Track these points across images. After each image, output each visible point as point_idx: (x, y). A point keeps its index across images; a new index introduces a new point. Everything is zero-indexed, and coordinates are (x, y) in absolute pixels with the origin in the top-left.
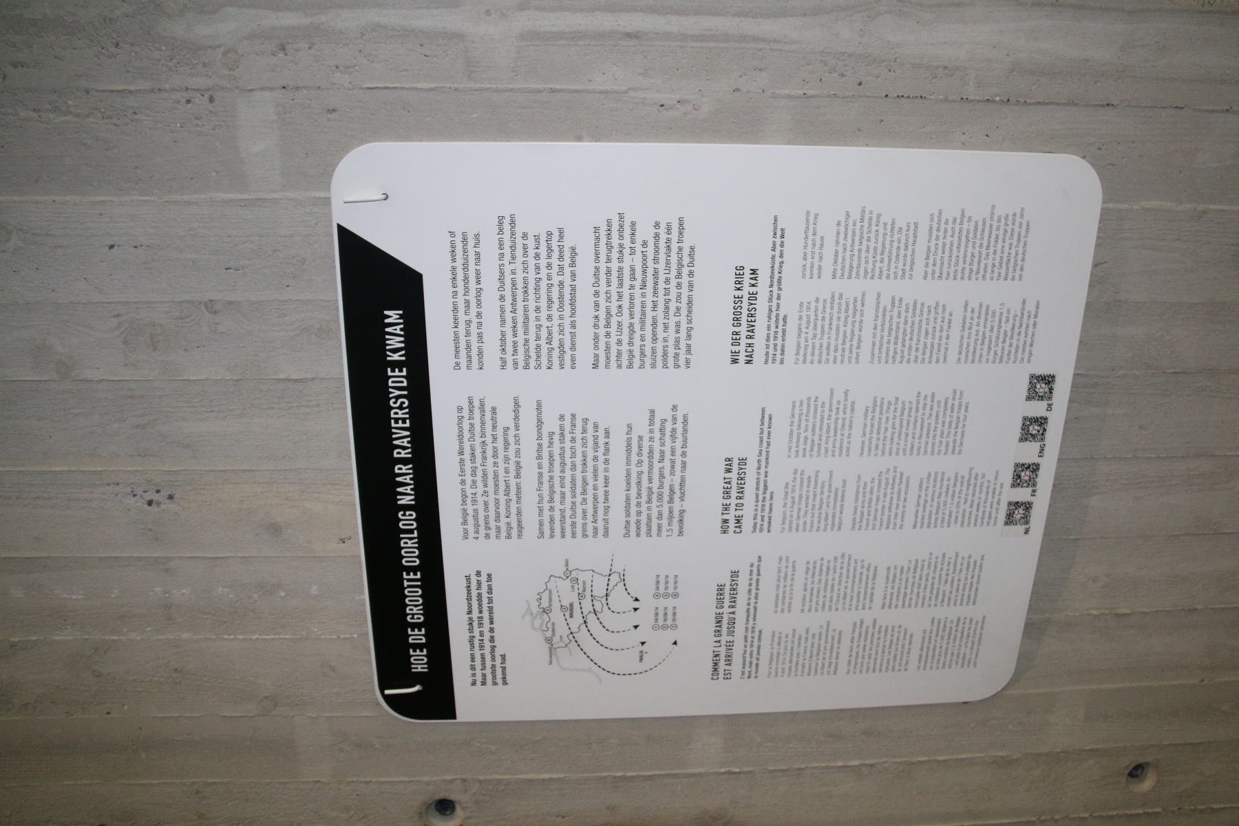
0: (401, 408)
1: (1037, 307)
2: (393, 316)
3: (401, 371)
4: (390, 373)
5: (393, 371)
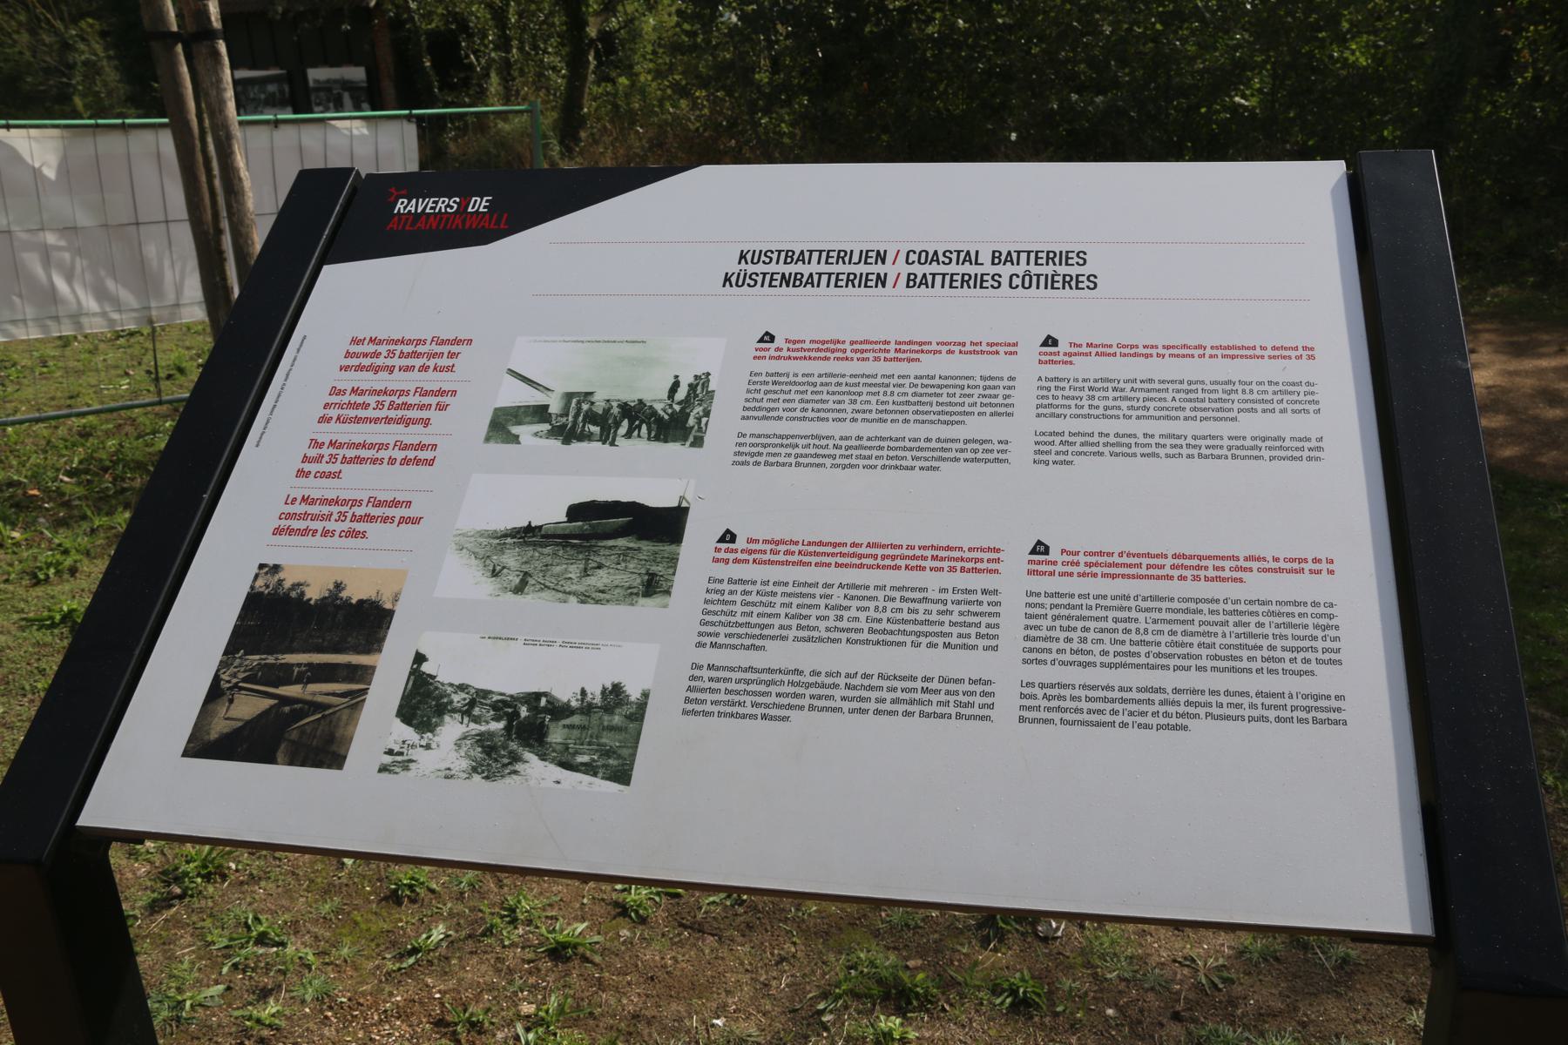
0: (448, 206)
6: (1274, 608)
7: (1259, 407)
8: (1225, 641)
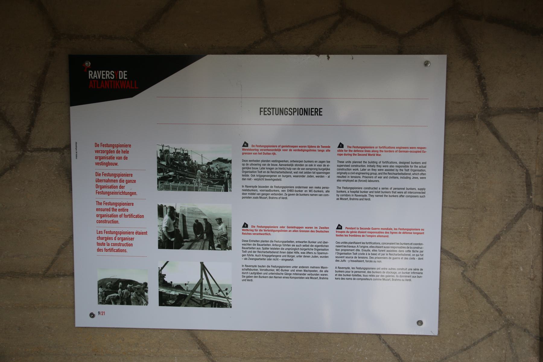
0: (110, 75)
1: (138, 216)
2: (123, 75)
3: (126, 77)
4: (124, 72)
5: (126, 73)
6: (252, 196)
7: (399, 176)
8: (369, 252)
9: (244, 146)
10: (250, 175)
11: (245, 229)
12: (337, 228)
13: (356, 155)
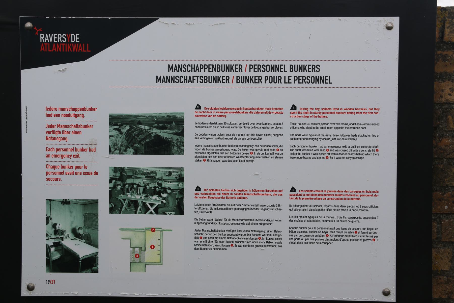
0: (62, 39)
2: (75, 38)
3: (78, 40)
4: (77, 35)
5: (78, 36)
9: (196, 108)
10: (237, 150)
11: (197, 192)
12: (291, 191)
13: (316, 117)
